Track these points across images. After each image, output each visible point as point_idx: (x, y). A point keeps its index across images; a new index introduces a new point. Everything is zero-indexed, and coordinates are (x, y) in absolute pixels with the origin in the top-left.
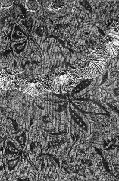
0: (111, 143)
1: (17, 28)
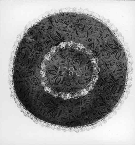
0: (50, 28)
1: (78, 27)
